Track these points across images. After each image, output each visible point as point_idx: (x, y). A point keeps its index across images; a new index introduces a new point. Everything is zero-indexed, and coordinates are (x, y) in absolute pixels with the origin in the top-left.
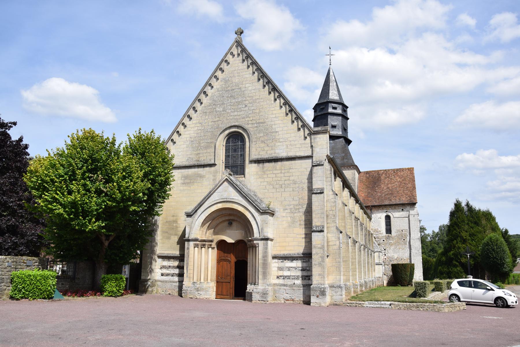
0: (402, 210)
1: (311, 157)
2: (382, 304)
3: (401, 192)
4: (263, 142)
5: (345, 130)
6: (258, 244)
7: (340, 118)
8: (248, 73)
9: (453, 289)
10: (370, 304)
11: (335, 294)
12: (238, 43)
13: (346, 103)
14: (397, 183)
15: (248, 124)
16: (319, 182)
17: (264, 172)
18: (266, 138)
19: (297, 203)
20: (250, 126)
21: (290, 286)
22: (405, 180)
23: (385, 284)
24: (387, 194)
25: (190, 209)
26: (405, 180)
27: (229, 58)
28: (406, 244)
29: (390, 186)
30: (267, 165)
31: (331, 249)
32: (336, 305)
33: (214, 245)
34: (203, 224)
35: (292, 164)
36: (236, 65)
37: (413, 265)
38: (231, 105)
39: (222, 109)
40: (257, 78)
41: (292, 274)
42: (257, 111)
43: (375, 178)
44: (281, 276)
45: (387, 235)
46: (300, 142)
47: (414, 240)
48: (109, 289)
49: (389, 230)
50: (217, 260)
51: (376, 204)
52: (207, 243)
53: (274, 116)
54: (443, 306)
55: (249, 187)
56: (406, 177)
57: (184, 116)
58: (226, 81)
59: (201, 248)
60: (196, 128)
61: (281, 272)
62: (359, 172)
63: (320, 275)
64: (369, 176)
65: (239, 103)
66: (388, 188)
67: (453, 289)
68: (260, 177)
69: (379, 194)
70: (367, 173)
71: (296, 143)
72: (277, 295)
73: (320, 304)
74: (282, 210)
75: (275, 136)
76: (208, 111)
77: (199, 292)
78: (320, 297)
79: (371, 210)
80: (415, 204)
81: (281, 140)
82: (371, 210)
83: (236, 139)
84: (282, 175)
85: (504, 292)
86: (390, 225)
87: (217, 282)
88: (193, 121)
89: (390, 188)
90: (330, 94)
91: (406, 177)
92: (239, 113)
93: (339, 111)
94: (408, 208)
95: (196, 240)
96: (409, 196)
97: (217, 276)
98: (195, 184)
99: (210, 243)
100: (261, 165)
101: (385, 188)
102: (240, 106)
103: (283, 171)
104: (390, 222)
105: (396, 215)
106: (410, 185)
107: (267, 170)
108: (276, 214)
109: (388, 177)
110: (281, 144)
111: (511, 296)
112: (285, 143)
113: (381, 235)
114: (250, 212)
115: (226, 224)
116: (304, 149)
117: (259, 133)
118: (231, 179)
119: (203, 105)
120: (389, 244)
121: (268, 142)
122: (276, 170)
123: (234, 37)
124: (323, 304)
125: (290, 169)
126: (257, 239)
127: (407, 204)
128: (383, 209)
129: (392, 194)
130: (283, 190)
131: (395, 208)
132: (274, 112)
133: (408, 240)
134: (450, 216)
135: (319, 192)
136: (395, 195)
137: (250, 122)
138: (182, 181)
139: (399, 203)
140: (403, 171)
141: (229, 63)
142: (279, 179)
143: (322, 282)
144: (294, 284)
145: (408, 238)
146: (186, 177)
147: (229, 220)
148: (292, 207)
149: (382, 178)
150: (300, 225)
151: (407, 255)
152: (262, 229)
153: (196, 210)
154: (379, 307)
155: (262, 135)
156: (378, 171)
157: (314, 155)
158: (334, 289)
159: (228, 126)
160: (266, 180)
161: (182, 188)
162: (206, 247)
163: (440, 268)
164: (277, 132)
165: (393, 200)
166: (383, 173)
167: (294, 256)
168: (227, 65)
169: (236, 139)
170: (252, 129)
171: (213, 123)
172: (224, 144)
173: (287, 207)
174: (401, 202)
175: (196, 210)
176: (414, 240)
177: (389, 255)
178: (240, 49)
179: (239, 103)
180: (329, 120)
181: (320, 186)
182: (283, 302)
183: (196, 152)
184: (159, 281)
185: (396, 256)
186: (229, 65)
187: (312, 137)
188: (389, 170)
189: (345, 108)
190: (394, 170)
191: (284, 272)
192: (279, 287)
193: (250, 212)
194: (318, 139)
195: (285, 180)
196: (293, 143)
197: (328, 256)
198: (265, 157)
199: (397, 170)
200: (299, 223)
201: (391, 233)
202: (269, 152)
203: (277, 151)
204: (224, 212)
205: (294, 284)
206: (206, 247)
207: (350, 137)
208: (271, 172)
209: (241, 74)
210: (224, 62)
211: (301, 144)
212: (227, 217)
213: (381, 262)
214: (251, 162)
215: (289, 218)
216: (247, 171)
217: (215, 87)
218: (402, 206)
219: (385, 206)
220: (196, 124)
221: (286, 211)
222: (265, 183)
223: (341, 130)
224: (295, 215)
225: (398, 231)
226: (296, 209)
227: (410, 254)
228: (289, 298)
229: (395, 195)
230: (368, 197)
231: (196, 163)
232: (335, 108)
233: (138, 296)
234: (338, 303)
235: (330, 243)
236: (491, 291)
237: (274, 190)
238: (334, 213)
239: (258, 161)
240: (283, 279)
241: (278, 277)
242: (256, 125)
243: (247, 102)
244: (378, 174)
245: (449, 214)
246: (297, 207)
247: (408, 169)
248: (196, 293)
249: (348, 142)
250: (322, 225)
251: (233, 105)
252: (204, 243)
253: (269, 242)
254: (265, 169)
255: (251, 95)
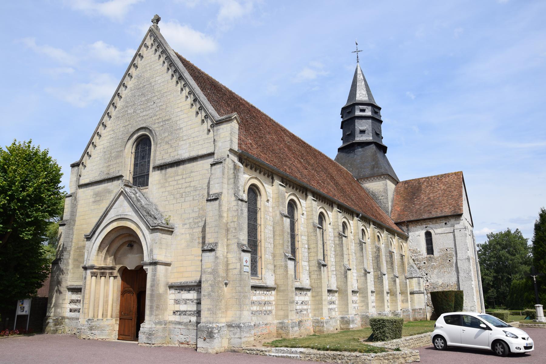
0: (446, 224)
1: (212, 154)
2: (292, 353)
3: (445, 202)
4: (167, 143)
5: (378, 134)
6: (147, 269)
7: (370, 121)
8: (158, 64)
9: (438, 328)
10: (278, 351)
11: (232, 336)
12: (153, 33)
13: (378, 104)
14: (440, 192)
15: (155, 124)
16: (217, 185)
17: (166, 179)
18: (170, 137)
19: (197, 215)
20: (156, 125)
21: (186, 324)
22: (450, 187)
23: (429, 318)
24: (427, 206)
25: (88, 232)
26: (450, 187)
27: (143, 50)
28: (452, 266)
29: (431, 195)
30: (170, 170)
31: (230, 274)
32: (234, 351)
33: (116, 273)
34: (100, 248)
35: (193, 166)
36: (149, 57)
37: (462, 292)
38: (141, 105)
39: (132, 111)
40: (166, 68)
41: (189, 309)
42: (164, 107)
43: (415, 188)
44: (177, 311)
45: (429, 256)
46: (203, 137)
47: (461, 260)
48: (223, 321)
49: (430, 250)
50: (121, 292)
51: (412, 219)
52: (108, 271)
53: (179, 110)
54: (369, 358)
55: (151, 200)
56: (455, 183)
57: (99, 125)
58: (139, 77)
59: (101, 277)
60: (109, 137)
61: (178, 305)
62: (395, 181)
63: (209, 309)
64: (408, 186)
65: (148, 100)
66: (429, 198)
67: (438, 328)
68: (162, 187)
69: (418, 207)
70: (406, 182)
71: (199, 139)
72: (172, 336)
73: (207, 349)
74: (181, 225)
75: (178, 134)
76: (120, 116)
77: (93, 331)
78: (208, 340)
79: (407, 226)
80: (461, 215)
81: (185, 138)
82: (407, 226)
83: (143, 144)
84: (183, 181)
85: (505, 332)
86: (431, 244)
87: (120, 319)
88: (108, 129)
89: (432, 198)
90: (358, 95)
91: (455, 183)
92: (147, 113)
93: (368, 113)
94: (452, 221)
95: (92, 267)
96: (454, 206)
97: (121, 312)
98: (104, 201)
99: (111, 271)
100: (163, 171)
101: (426, 198)
102: (149, 104)
103: (184, 177)
104: (431, 240)
105: (439, 232)
106: (455, 193)
107: (169, 177)
108: (176, 231)
109: (431, 186)
110: (184, 142)
111: (517, 337)
112: (188, 141)
113: (420, 257)
114: (141, 230)
115: (126, 247)
116: (207, 146)
117: (164, 133)
118: (125, 191)
119: (117, 109)
120: (432, 268)
121: (173, 142)
122: (178, 175)
123: (149, 25)
124: (210, 351)
125: (192, 172)
126: (147, 264)
127: (451, 216)
128: (422, 224)
129: (433, 205)
130: (183, 200)
131: (436, 223)
132: (180, 105)
133: (455, 261)
134: (535, 229)
135: (214, 198)
136: (436, 206)
137: (157, 121)
138: (93, 200)
139: (440, 215)
140: (449, 177)
141: (142, 57)
142: (180, 186)
143: (211, 319)
144: (190, 321)
145: (454, 258)
146: (97, 194)
147: (131, 241)
148: (191, 220)
149: (423, 187)
150: (199, 243)
151: (454, 279)
152: (151, 251)
153: (94, 232)
154: (287, 357)
155: (166, 134)
156: (419, 179)
157: (216, 152)
158: (232, 329)
159: (137, 128)
160: (168, 189)
161: (92, 207)
162: (99, 276)
163: (526, 294)
164: (181, 129)
165: (433, 213)
166: (424, 181)
167: (191, 284)
168: (141, 60)
169: (143, 144)
170: (158, 129)
171: (124, 128)
172: (133, 151)
173: (187, 221)
174: (443, 215)
175: (94, 232)
176: (461, 260)
177: (432, 281)
178: (153, 38)
179: (148, 100)
180: (356, 124)
181: (217, 191)
182: (177, 345)
183: (107, 165)
184: (68, 318)
185: (440, 282)
186: (143, 59)
187: (215, 128)
188: (432, 177)
189: (376, 109)
190: (437, 177)
191: (181, 306)
192: (174, 326)
193: (141, 230)
194: (221, 131)
195: (186, 188)
196: (196, 139)
197: (226, 284)
198: (168, 161)
199: (442, 176)
200: (197, 241)
201: (433, 254)
202: (172, 155)
203: (180, 152)
204: (121, 232)
205: (190, 321)
206: (99, 276)
207: (384, 142)
208: (173, 178)
209: (153, 66)
210: (138, 56)
211: (204, 140)
212: (124, 240)
213: (422, 289)
214: (154, 168)
215: (188, 235)
216: (151, 180)
217: (128, 87)
218: (445, 218)
219: (424, 220)
220: (110, 131)
221: (185, 226)
222: (167, 193)
223: (371, 135)
224: (194, 231)
225: (442, 250)
226: (195, 223)
227: (458, 278)
228: (183, 340)
229: (436, 206)
230: (404, 211)
231: (106, 177)
232: (363, 111)
233: (31, 337)
234: (236, 349)
235: (231, 267)
236: (487, 331)
237: (174, 201)
238: (236, 226)
239: (161, 167)
240: (180, 315)
241: (174, 313)
242: (162, 124)
243: (156, 98)
244: (419, 183)
245: (533, 227)
246: (197, 221)
247: (456, 174)
248: (89, 332)
249: (384, 149)
250: (216, 241)
251: (143, 104)
252: (102, 271)
253: (159, 267)
254: (167, 176)
255: (160, 89)
